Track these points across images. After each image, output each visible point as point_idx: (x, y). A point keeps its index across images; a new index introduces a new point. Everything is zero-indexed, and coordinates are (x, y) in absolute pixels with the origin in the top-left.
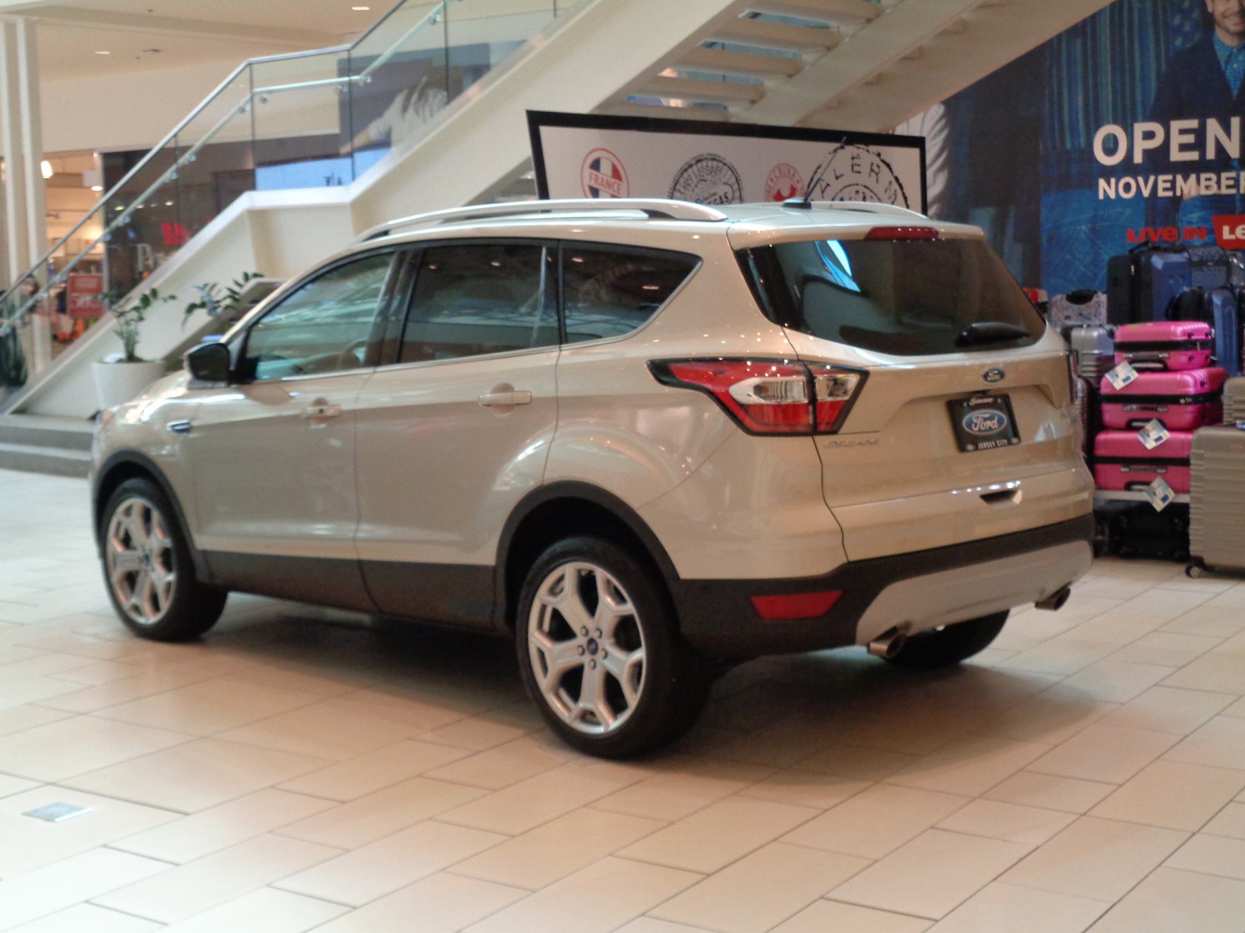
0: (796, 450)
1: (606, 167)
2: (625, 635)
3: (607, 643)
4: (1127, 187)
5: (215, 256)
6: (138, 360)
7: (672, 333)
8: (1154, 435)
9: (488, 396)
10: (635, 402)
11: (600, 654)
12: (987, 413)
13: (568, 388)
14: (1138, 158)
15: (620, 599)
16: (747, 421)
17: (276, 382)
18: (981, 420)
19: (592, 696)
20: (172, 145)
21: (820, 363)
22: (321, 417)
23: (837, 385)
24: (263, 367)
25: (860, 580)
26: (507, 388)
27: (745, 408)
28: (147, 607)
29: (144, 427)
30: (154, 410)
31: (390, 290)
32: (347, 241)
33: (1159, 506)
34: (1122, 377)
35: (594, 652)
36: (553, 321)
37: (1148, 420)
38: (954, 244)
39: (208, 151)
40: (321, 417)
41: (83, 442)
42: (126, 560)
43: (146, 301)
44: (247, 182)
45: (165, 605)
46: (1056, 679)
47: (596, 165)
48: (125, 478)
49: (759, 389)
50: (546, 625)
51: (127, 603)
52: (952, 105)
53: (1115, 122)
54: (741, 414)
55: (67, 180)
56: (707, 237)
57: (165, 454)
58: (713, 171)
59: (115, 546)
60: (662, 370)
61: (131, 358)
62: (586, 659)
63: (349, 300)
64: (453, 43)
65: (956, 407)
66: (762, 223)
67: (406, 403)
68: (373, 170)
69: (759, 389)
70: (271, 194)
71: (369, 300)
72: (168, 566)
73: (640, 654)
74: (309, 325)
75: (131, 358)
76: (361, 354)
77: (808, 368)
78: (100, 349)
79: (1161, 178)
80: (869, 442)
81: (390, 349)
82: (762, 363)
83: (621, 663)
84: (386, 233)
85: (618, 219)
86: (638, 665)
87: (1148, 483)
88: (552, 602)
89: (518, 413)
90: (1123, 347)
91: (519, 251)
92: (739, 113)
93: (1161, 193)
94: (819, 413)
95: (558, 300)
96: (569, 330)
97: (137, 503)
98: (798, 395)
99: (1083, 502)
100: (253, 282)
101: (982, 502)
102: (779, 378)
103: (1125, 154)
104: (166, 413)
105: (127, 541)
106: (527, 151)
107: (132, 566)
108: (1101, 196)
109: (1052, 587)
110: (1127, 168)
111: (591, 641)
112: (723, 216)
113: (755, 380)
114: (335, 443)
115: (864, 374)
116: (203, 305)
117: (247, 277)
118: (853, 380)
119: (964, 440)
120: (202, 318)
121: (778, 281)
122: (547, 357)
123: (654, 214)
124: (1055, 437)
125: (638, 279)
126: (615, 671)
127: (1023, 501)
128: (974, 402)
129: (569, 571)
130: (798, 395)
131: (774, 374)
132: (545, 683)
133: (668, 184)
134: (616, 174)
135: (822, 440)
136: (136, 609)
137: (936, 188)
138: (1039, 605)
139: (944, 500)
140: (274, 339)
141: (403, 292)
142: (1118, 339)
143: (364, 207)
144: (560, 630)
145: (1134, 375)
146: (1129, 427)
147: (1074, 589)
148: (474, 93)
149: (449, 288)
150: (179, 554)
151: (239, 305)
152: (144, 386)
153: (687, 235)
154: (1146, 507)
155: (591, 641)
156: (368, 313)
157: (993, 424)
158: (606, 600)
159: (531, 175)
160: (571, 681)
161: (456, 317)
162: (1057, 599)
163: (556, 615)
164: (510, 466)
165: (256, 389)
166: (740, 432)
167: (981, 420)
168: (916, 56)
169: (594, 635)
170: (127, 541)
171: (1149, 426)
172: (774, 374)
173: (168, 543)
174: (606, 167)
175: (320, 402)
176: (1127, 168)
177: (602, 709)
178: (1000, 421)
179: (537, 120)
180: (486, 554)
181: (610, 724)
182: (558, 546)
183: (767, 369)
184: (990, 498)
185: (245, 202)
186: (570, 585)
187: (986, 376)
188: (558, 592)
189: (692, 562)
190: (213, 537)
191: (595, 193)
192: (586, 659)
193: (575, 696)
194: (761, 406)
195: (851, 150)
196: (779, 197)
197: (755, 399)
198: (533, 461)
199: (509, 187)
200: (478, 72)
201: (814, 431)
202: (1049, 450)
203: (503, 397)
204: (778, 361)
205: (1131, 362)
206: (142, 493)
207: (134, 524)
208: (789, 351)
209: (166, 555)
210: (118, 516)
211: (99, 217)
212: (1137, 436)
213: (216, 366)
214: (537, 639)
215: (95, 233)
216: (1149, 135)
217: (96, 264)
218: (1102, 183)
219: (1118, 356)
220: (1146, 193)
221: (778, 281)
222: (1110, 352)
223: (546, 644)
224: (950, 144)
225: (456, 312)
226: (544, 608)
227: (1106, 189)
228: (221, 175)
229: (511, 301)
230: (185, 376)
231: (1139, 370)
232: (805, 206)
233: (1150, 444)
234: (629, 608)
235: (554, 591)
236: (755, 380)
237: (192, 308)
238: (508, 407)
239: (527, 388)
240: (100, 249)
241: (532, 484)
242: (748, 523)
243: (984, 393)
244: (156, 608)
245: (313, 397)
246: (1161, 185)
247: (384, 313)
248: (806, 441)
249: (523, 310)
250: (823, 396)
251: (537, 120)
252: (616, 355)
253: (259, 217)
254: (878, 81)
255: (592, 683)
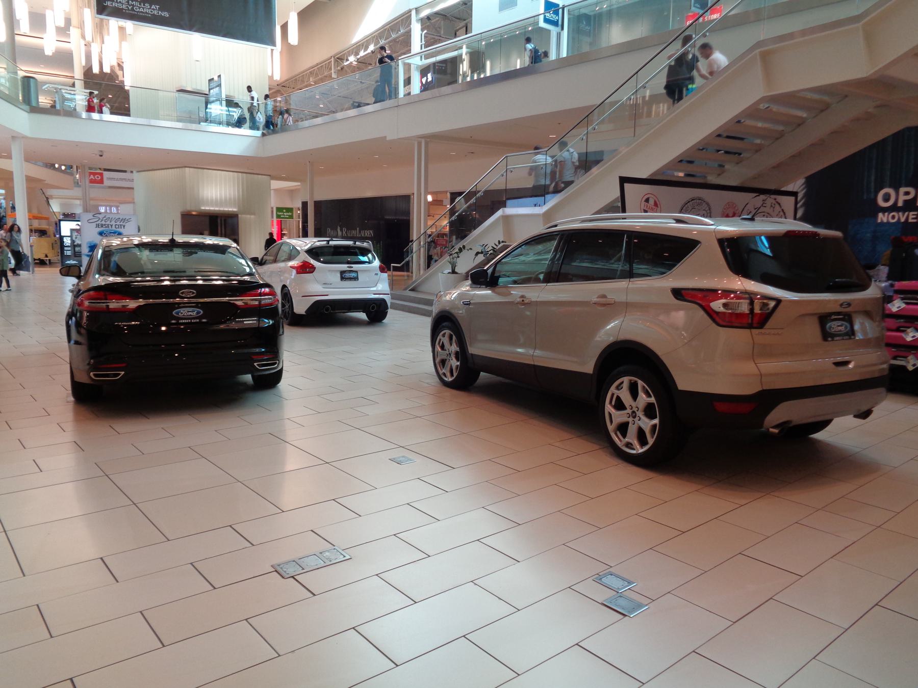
0: (740, 337)
1: (651, 202)
2: (649, 411)
3: (640, 414)
4: (893, 217)
5: (488, 233)
6: (456, 273)
7: (684, 276)
8: (911, 334)
9: (595, 299)
10: (667, 309)
11: (637, 418)
12: (840, 323)
13: (632, 298)
14: (900, 204)
15: (649, 396)
16: (718, 319)
17: (505, 287)
18: (835, 326)
19: (632, 437)
20: (474, 190)
21: (756, 294)
22: (523, 303)
23: (765, 305)
24: (501, 280)
25: (769, 398)
26: (604, 296)
27: (717, 313)
28: (448, 374)
29: (451, 301)
30: (455, 293)
31: (556, 250)
32: (539, 229)
33: (910, 368)
34: (897, 306)
35: (634, 417)
36: (627, 267)
37: (909, 327)
38: (826, 239)
39: (486, 192)
40: (523, 303)
41: (430, 303)
42: (442, 354)
43: (460, 250)
44: (504, 205)
45: (455, 374)
46: (858, 450)
47: (647, 200)
48: (444, 322)
49: (725, 305)
50: (613, 403)
51: (441, 372)
52: (811, 181)
53: (890, 187)
54: (715, 316)
55: (437, 202)
56: (700, 232)
57: (460, 313)
58: (699, 204)
59: (438, 348)
60: (678, 293)
61: (454, 272)
62: (630, 420)
63: (539, 253)
64: (591, 149)
65: (823, 319)
66: (729, 228)
67: (560, 299)
68: (552, 201)
69: (725, 305)
70: (512, 210)
71: (545, 255)
72: (457, 359)
73: (656, 421)
74: (524, 263)
75: (454, 272)
76: (541, 277)
77: (751, 297)
78: (442, 267)
79: (911, 213)
80: (778, 334)
81: (553, 276)
82: (727, 293)
83: (647, 424)
84: (556, 226)
85: (663, 222)
86: (654, 426)
87: (906, 357)
88: (617, 392)
89: (608, 308)
90: (898, 292)
91: (613, 237)
92: (712, 179)
93: (910, 220)
94: (758, 318)
95: (630, 258)
96: (635, 271)
97: (447, 332)
98: (744, 307)
99: (883, 369)
100: (502, 244)
101: (834, 366)
102: (735, 301)
103: (892, 203)
104: (460, 296)
105: (442, 347)
106: (618, 194)
107: (444, 357)
108: (879, 221)
109: (864, 408)
110: (894, 208)
111: (634, 412)
112: (712, 223)
113: (723, 301)
114: (528, 313)
115: (779, 301)
116: (482, 253)
117: (499, 242)
118: (772, 304)
119: (827, 336)
120: (481, 258)
121: (738, 254)
122: (623, 284)
123: (678, 221)
124: (870, 336)
125: (667, 251)
126: (643, 426)
127: (855, 367)
128: (833, 317)
129: (626, 380)
130: (744, 307)
131: (732, 298)
132: (611, 428)
133: (679, 208)
134: (656, 204)
135: (755, 331)
136: (444, 374)
137: (800, 213)
138: (855, 416)
139: (816, 366)
140: (506, 268)
141: (562, 252)
142: (896, 288)
143: (547, 215)
144: (620, 405)
145: (903, 306)
146: (898, 330)
147: (876, 410)
148: (595, 171)
149: (582, 252)
150: (463, 354)
151: (495, 252)
152: (455, 286)
153: (691, 231)
154: (904, 368)
155: (634, 412)
156: (546, 260)
157: (842, 328)
158: (642, 396)
159: (620, 204)
160: (623, 428)
161: (583, 264)
162: (865, 415)
163: (618, 398)
164: (602, 332)
165: (497, 290)
166: (714, 325)
167: (835, 326)
168: (799, 155)
169: (635, 409)
170: (442, 347)
171: (909, 330)
172: (732, 298)
173: (458, 349)
174: (651, 202)
175: (522, 297)
176: (894, 208)
177: (636, 443)
178: (846, 327)
179: (623, 180)
180: (588, 367)
181: (639, 450)
182: (621, 368)
183: (729, 296)
184: (838, 364)
185: (499, 213)
186: (626, 386)
187: (841, 305)
188: (620, 389)
189: (684, 383)
190: (474, 349)
191: (645, 211)
192: (630, 420)
193: (624, 436)
194: (724, 313)
195: (762, 197)
196: (727, 216)
197: (722, 309)
198: (613, 329)
199: (610, 208)
200: (597, 162)
201: (750, 326)
202: (866, 343)
203: (602, 300)
204: (734, 292)
205: (903, 299)
206: (449, 329)
207: (446, 340)
208: (741, 288)
209: (457, 354)
210: (440, 337)
211: (448, 216)
212: (903, 335)
213: (480, 278)
214: (609, 408)
215: (445, 222)
216: (907, 193)
217: (445, 234)
218: (880, 215)
219: (895, 296)
220: (903, 220)
221: (738, 254)
222: (891, 294)
223: (613, 411)
224: (806, 195)
225: (582, 261)
226: (613, 395)
227: (882, 218)
228: (493, 201)
229: (607, 257)
230: (469, 282)
231: (907, 303)
232: (752, 219)
233: (909, 339)
234: (653, 400)
235: (619, 388)
236: (723, 301)
237: (477, 254)
238: (604, 305)
239: (611, 297)
240: (448, 229)
241: (612, 339)
242: (714, 367)
243: (839, 313)
244: (452, 375)
245: (521, 294)
246: (911, 217)
247: (552, 260)
248: (747, 331)
249: (612, 261)
250: (757, 310)
251: (623, 180)
252: (656, 285)
253: (506, 219)
254: (778, 166)
255: (632, 430)
